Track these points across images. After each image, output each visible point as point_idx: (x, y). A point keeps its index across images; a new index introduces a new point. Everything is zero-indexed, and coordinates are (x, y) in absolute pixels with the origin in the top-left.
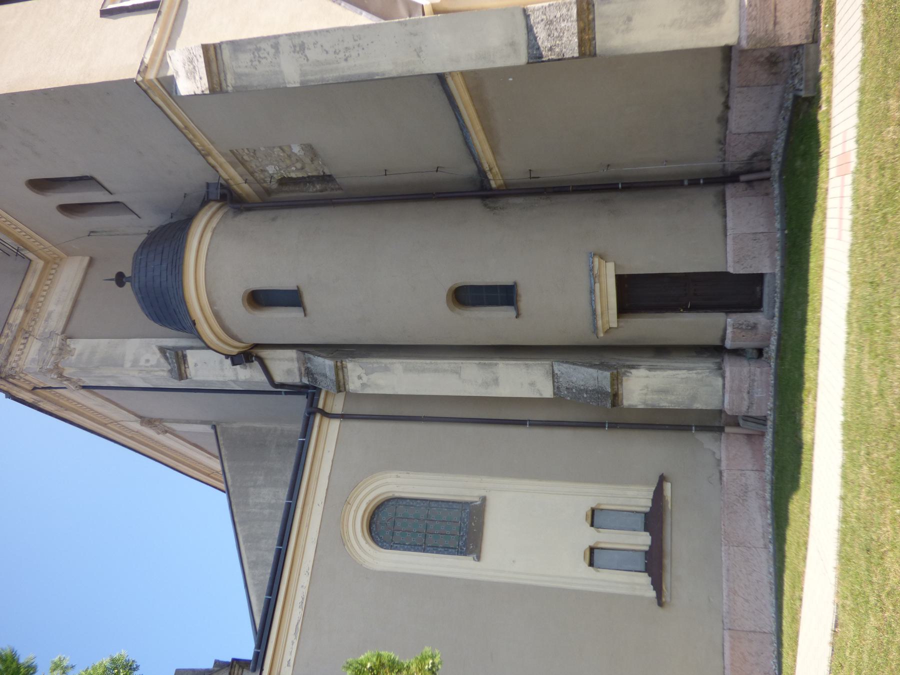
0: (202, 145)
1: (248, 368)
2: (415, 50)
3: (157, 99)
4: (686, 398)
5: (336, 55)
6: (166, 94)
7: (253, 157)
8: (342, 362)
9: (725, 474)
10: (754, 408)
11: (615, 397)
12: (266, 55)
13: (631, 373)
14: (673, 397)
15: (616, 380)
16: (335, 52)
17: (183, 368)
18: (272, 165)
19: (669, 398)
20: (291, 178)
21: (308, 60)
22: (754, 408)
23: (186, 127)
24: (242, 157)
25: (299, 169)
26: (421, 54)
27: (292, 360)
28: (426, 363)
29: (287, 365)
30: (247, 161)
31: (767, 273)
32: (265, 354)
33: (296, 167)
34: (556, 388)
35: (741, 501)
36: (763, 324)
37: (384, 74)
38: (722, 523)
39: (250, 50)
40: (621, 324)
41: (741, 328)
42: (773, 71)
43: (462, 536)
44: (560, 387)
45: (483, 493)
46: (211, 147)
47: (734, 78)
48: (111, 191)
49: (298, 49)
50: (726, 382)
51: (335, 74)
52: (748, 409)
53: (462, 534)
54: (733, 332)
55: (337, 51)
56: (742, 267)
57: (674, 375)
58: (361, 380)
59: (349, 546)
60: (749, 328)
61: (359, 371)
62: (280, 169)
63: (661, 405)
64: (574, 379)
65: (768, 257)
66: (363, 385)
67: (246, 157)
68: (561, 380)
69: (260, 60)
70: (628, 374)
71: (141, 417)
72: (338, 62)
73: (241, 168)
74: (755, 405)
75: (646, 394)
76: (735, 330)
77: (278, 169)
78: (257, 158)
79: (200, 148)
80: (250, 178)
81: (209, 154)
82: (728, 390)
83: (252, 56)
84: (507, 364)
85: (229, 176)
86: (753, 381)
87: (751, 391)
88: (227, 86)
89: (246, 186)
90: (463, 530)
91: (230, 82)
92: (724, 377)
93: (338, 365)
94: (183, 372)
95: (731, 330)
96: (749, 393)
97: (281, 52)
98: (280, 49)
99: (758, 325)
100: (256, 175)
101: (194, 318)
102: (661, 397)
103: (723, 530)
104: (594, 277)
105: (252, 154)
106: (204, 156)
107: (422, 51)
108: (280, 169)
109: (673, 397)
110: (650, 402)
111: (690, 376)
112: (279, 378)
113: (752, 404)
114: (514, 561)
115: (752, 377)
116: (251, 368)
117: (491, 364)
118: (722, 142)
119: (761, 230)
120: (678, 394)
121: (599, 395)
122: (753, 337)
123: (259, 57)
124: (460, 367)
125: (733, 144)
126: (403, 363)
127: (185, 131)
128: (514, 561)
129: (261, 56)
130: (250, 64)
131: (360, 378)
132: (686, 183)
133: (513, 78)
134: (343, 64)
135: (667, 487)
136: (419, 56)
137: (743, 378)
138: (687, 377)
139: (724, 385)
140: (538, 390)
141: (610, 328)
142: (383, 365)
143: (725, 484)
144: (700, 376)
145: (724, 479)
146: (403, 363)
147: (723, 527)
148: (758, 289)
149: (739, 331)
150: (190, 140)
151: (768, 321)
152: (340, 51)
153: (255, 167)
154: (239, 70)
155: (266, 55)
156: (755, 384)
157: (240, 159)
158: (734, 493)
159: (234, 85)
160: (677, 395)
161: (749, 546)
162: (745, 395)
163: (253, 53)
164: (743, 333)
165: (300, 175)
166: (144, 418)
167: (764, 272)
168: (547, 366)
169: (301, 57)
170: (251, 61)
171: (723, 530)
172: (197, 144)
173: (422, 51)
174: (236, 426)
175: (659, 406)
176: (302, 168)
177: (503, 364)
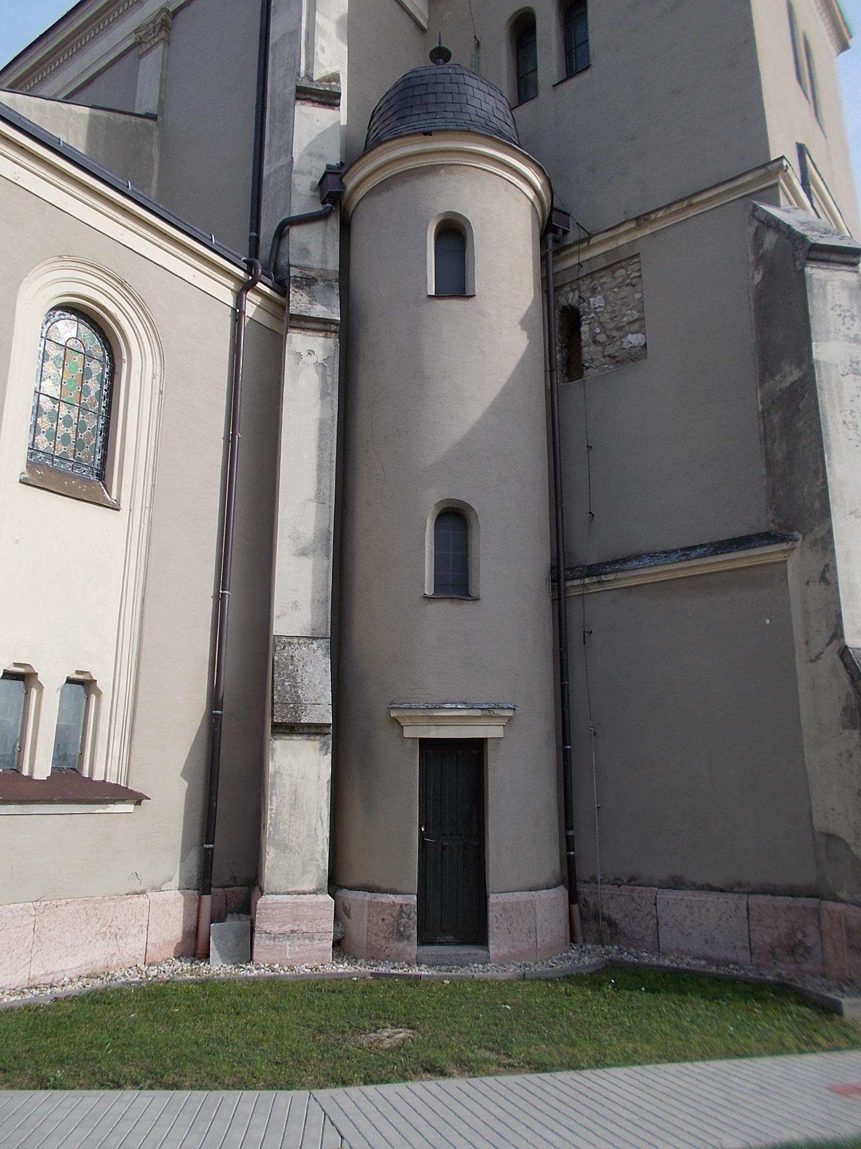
0: (657, 220)
1: (312, 193)
2: (857, 510)
3: (749, 178)
4: (284, 835)
5: (849, 412)
6: (750, 191)
7: (623, 281)
8: (335, 332)
9: (142, 899)
10: (267, 942)
11: (291, 729)
12: (847, 325)
13: (326, 754)
14: (286, 816)
15: (313, 730)
16: (852, 411)
17: (315, 98)
18: (606, 304)
19: (285, 810)
20: (579, 325)
21: (843, 375)
22: (267, 942)
23: (691, 206)
24: (622, 267)
25: (594, 337)
26: (853, 516)
27: (324, 261)
28: (331, 455)
29: (315, 247)
30: (614, 272)
31: (488, 951)
32: (334, 224)
33: (599, 333)
34: (289, 640)
35: (104, 929)
36: (408, 948)
37: (830, 466)
38: (69, 900)
39: (852, 307)
40: (409, 744)
41: (402, 917)
42: (778, 950)
43: (53, 460)
44: (292, 646)
45: (125, 505)
46: (648, 231)
47: (763, 900)
48: (560, 87)
49: (855, 366)
50: (308, 896)
51: (828, 406)
52: (266, 932)
53: (55, 460)
54: (394, 904)
55: (853, 414)
56: (498, 915)
57: (321, 818)
58: (307, 354)
59: (56, 265)
60: (402, 929)
61: (320, 356)
62: (596, 313)
63: (274, 798)
64: (309, 669)
65: (510, 952)
66: (299, 355)
67: (621, 273)
68: (304, 649)
69: (842, 317)
70: (324, 752)
71: (175, 13)
72: (841, 411)
73: (603, 263)
74: (272, 943)
75: (291, 776)
76: (398, 907)
77: (598, 310)
78: (620, 287)
79: (653, 217)
80: (584, 272)
81: (639, 227)
82: (298, 901)
83: (846, 308)
84: (327, 571)
85: (593, 244)
86: (312, 938)
87: (295, 934)
88: (812, 268)
89: (574, 261)
90: (62, 463)
91: (816, 273)
92: (315, 892)
93: (332, 326)
94: (308, 96)
95: (396, 901)
96: (293, 932)
97: (850, 345)
98: (854, 345)
99: (405, 942)
100: (588, 281)
101: (434, 136)
102: (287, 798)
103: (59, 902)
104: (489, 712)
105: (628, 281)
106: (637, 219)
107: (856, 518)
108: (596, 313)
109: (286, 816)
110: (278, 781)
111: (320, 842)
112: (296, 233)
113: (274, 938)
114: (17, 541)
115: (318, 936)
116: (313, 197)
117: (328, 548)
118: (633, 880)
119: (539, 940)
120: (292, 824)
121: (291, 705)
122: (382, 935)
123: (845, 317)
124: (324, 503)
125: (635, 895)
126: (333, 420)
127: (686, 203)
128: (17, 541)
129: (846, 320)
130: (837, 303)
131: (311, 353)
132: (570, 833)
133: (769, 625)
134: (839, 418)
135: (129, 808)
136: (851, 513)
137: (317, 922)
138: (317, 837)
139: (304, 893)
140: (285, 614)
141: (402, 726)
142: (329, 391)
143: (129, 901)
144: (318, 856)
145: (136, 899)
146: (333, 420)
147: (64, 901)
148: (450, 938)
149: (395, 914)
150: (668, 206)
151: (414, 957)
152: (854, 417)
153: (602, 281)
154: (829, 287)
155: (847, 325)
156: (307, 942)
157: (624, 264)
158: (116, 917)
159: (813, 276)
160: (290, 822)
161: (34, 951)
162: (287, 928)
163: (848, 310)
164: (389, 920)
165: (585, 337)
166: (173, 18)
167: (491, 947)
168: (323, 631)
169: (846, 367)
170: (840, 306)
171: (59, 902)
172: (660, 214)
173: (856, 518)
174: (155, 151)
175: (272, 794)
176: (595, 342)
177: (328, 566)
